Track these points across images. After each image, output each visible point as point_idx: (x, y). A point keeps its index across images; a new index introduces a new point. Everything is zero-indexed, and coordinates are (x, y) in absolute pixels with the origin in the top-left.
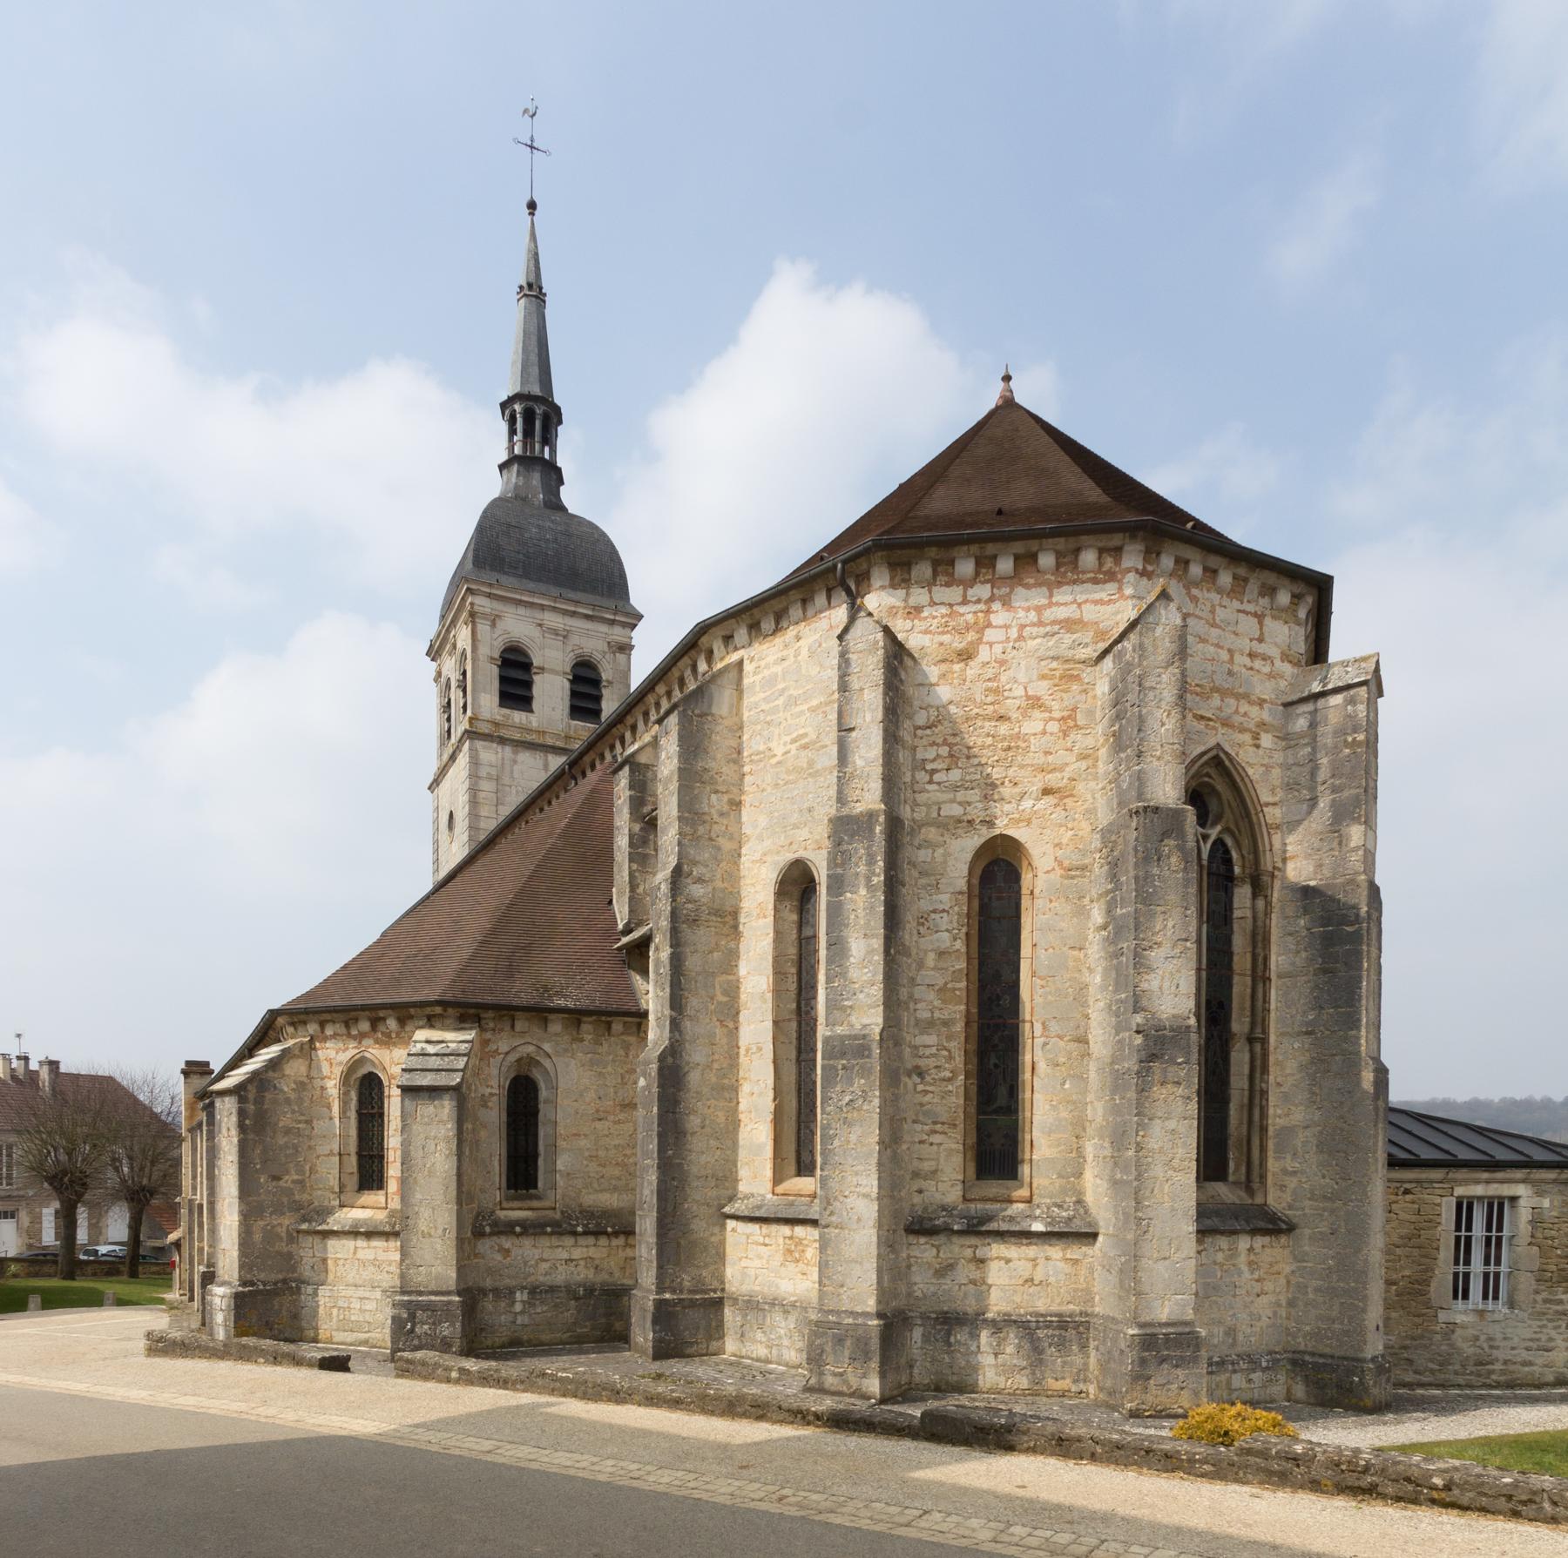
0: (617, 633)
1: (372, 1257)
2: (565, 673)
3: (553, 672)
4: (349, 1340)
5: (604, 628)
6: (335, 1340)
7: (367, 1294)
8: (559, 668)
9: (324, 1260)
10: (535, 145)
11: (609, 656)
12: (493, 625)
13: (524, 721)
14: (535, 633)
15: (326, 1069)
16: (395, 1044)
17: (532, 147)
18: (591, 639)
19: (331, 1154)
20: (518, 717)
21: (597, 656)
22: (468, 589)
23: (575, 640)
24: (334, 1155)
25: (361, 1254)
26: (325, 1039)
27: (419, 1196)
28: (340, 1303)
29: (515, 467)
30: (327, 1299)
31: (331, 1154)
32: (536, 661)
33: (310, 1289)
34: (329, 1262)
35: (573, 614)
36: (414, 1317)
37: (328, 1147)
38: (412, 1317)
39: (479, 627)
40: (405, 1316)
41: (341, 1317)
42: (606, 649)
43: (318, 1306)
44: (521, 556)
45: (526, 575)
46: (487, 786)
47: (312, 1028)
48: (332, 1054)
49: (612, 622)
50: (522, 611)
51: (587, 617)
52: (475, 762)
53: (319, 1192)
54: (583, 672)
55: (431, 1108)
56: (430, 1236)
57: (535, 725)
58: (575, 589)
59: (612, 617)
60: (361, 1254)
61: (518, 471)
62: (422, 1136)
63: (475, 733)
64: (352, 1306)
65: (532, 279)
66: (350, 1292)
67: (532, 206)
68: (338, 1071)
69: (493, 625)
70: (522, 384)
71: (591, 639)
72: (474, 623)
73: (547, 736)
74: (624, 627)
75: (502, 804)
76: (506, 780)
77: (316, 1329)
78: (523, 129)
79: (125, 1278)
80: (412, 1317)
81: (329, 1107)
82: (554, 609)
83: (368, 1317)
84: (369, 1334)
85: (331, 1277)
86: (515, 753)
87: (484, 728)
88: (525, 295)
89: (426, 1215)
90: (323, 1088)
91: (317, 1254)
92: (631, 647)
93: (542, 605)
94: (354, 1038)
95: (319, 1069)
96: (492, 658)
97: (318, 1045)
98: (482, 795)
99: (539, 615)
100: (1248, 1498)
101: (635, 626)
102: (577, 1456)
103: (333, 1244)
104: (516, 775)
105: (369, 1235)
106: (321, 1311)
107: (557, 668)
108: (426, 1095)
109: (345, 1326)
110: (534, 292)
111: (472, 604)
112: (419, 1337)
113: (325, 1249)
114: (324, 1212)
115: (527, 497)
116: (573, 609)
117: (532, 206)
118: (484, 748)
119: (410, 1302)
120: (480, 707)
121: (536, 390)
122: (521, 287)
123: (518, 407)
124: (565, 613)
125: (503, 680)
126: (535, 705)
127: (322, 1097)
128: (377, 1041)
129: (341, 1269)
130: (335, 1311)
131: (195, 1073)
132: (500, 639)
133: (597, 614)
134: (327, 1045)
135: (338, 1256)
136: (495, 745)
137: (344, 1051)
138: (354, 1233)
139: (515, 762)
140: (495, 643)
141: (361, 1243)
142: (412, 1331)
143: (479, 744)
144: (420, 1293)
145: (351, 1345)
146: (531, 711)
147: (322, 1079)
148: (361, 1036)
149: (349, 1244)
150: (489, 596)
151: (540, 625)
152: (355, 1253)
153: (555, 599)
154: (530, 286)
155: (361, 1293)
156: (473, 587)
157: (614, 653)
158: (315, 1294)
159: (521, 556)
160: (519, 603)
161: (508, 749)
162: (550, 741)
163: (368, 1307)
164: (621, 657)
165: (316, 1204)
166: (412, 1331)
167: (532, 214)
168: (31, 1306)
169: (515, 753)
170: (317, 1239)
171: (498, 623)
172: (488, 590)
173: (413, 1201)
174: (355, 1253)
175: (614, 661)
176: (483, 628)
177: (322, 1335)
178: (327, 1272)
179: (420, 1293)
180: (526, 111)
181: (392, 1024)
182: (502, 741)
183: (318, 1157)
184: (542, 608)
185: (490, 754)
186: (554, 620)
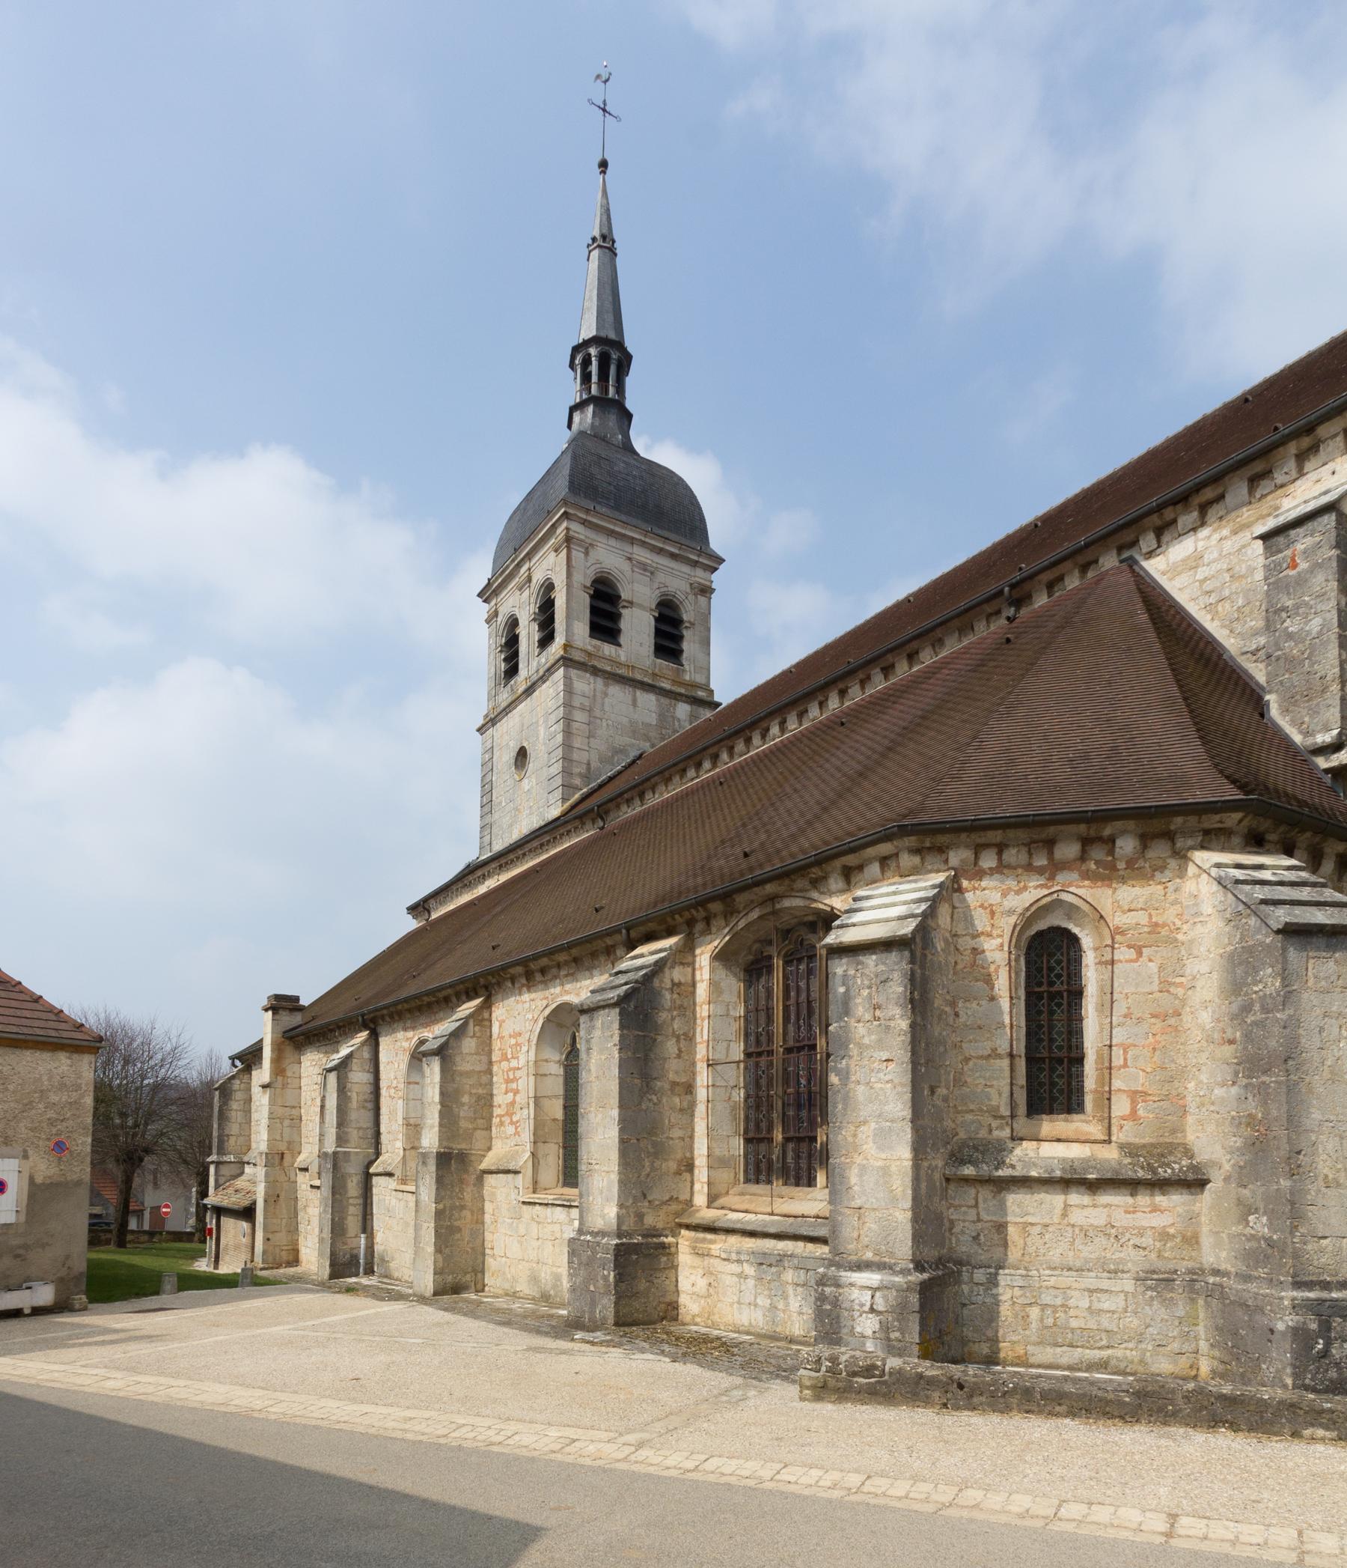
0: (699, 575)
1: (1101, 1221)
2: (651, 610)
3: (641, 607)
4: (1064, 1360)
5: (686, 569)
6: (1032, 1360)
7: (1105, 1284)
8: (646, 604)
9: (1001, 1228)
10: (607, 108)
11: (691, 597)
12: (587, 554)
13: (613, 655)
14: (626, 566)
15: (981, 921)
16: (1123, 880)
17: (604, 110)
18: (676, 579)
19: (994, 1054)
20: (608, 649)
21: (681, 596)
22: (565, 513)
23: (661, 577)
24: (1000, 1056)
25: (1077, 1217)
26: (980, 874)
27: (1316, 1115)
28: (1046, 1299)
29: (591, 408)
30: (1017, 1292)
31: (994, 1054)
32: (624, 595)
33: (980, 1275)
34: (1011, 1229)
35: (660, 551)
36: (1329, 1329)
37: (988, 1045)
38: (1326, 1327)
39: (574, 553)
40: (1314, 1326)
41: (1050, 1321)
42: (688, 590)
43: (997, 1303)
44: (612, 488)
45: (617, 508)
46: (579, 716)
47: (956, 857)
48: (994, 897)
49: (695, 564)
50: (612, 542)
51: (673, 556)
52: (569, 690)
53: (969, 1117)
54: (667, 612)
55: (1331, 964)
56: (1339, 1185)
57: (623, 659)
58: (661, 527)
59: (696, 558)
60: (1077, 1217)
61: (594, 412)
62: (1318, 1011)
63: (571, 660)
64: (1072, 1303)
65: (605, 231)
66: (1067, 1279)
67: (604, 165)
68: (1007, 924)
69: (587, 554)
70: (598, 329)
71: (676, 579)
72: (568, 548)
73: (636, 671)
74: (705, 570)
75: (593, 737)
76: (598, 713)
77: (995, 1341)
78: (597, 91)
79: (112, 1247)
80: (1326, 1327)
81: (988, 980)
82: (643, 544)
83: (1106, 1322)
84: (1110, 1352)
85: (1014, 1254)
86: (606, 685)
87: (577, 656)
88: (599, 246)
89: (1330, 1146)
90: (976, 951)
91: (984, 1216)
92: (713, 591)
93: (633, 538)
94: (1040, 871)
95: (968, 920)
96: (585, 587)
97: (965, 883)
98: (575, 725)
99: (628, 548)
100: (362, 1376)
101: (716, 569)
102: (365, 1408)
103: (1016, 1202)
104: (607, 708)
105: (1094, 1186)
106: (1005, 1310)
107: (645, 604)
108: (1322, 941)
109: (1053, 1336)
110: (606, 243)
111: (567, 529)
112: (1337, 1364)
113: (1002, 1208)
114: (996, 1152)
115: (605, 436)
116: (661, 545)
117: (604, 165)
118: (579, 677)
119: (1321, 1301)
120: (573, 634)
121: (612, 336)
122: (594, 239)
123: (593, 351)
124: (654, 549)
125: (594, 610)
126: (623, 639)
127: (974, 964)
128: (1086, 875)
129: (1034, 1242)
130: (1034, 1312)
131: (284, 1009)
132: (593, 568)
133: (681, 553)
134: (984, 884)
135: (1030, 1219)
136: (588, 675)
137: (1018, 892)
138: (1070, 1181)
139: (606, 694)
140: (588, 572)
141: (1075, 1198)
142: (1325, 1354)
143: (574, 673)
144: (1326, 1286)
145: (1070, 1368)
146: (619, 645)
147: (975, 936)
148: (1054, 868)
149: (1055, 1200)
150: (584, 523)
151: (630, 559)
152: (1064, 1215)
153: (646, 533)
154: (604, 237)
155: (1090, 1281)
156: (571, 511)
157: (695, 595)
158: (993, 1282)
159: (612, 488)
160: (611, 533)
161: (600, 681)
162: (639, 677)
163: (1106, 1306)
164: (702, 599)
165: (962, 1135)
166: (1325, 1354)
167: (604, 172)
168: (168, 1287)
169: (606, 685)
170: (985, 1193)
171: (592, 553)
172: (584, 516)
173: (1307, 1123)
174: (1064, 1215)
175: (696, 603)
176: (578, 555)
177: (1005, 1350)
178: (1006, 1245)
179: (1326, 1286)
180: (598, 77)
181: (1127, 845)
182: (596, 671)
183: (967, 1060)
184: (632, 541)
185: (584, 684)
186: (642, 554)
